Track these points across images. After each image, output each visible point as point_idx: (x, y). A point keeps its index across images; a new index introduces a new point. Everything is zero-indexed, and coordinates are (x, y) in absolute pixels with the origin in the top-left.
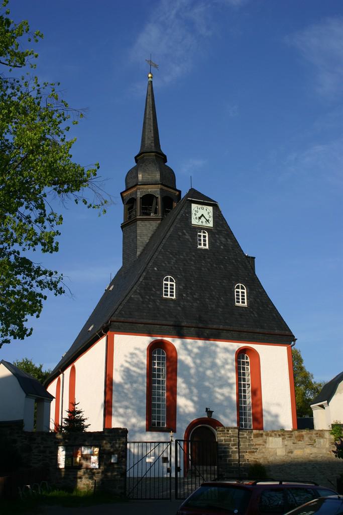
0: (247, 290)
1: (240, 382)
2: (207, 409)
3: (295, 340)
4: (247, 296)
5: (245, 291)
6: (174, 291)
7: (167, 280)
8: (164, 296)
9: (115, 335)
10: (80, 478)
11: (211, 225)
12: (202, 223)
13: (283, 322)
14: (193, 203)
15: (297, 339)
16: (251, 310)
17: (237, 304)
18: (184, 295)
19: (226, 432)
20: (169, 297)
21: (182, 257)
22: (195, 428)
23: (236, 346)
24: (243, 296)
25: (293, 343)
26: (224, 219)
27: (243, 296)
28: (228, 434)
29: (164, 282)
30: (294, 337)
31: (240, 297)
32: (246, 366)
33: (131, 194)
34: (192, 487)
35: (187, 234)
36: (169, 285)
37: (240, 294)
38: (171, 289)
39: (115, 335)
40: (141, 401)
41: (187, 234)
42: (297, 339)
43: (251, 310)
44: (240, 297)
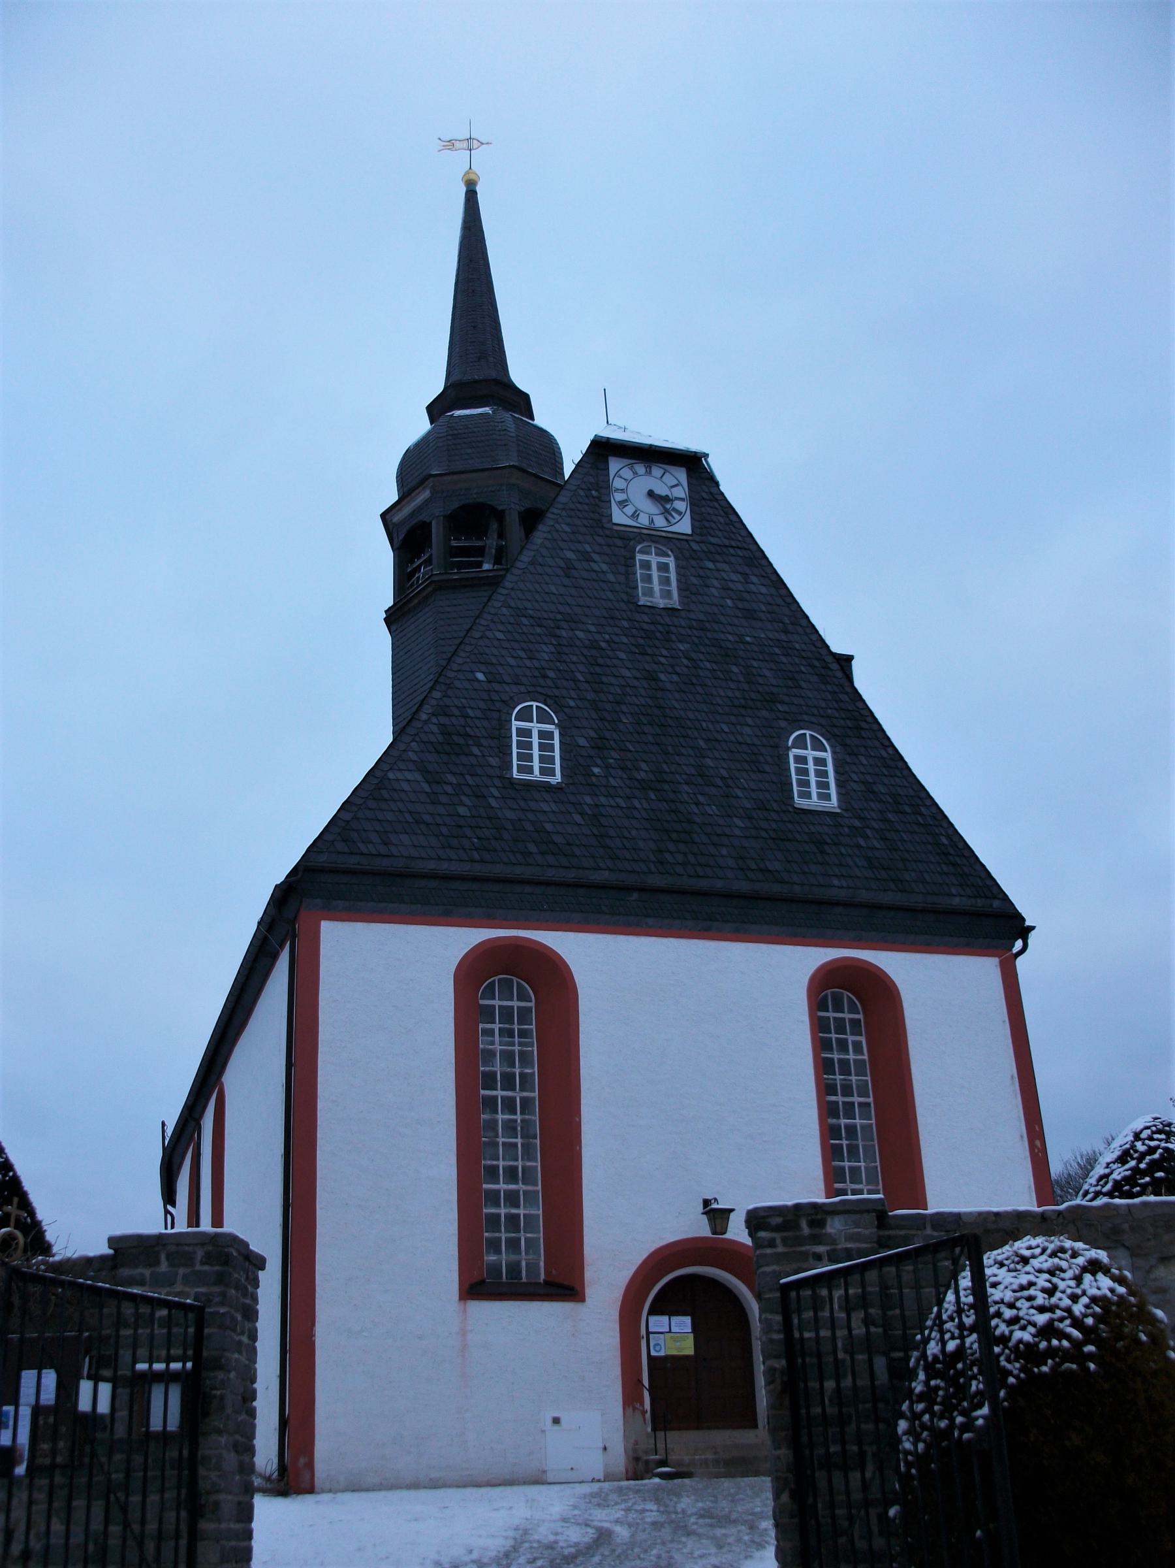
0: (834, 753)
1: (832, 1121)
2: (706, 1203)
3: (1024, 932)
4: (836, 772)
5: (828, 756)
6: (557, 754)
7: (525, 715)
8: (515, 774)
9: (325, 925)
10: (539, 1542)
11: (684, 526)
12: (648, 515)
13: (978, 867)
14: (615, 455)
15: (1033, 928)
16: (857, 823)
17: (799, 802)
18: (596, 770)
19: (806, 1230)
20: (536, 775)
21: (581, 635)
22: (484, 986)
23: (814, 957)
24: (822, 774)
25: (1019, 944)
26: (733, 509)
27: (822, 774)
28: (816, 1239)
29: (515, 724)
30: (1023, 920)
31: (813, 779)
32: (851, 1038)
33: (412, 514)
34: (900, 1447)
35: (596, 557)
36: (535, 734)
37: (811, 767)
38: (542, 747)
39: (325, 925)
40: (765, 1505)
41: (596, 557)
42: (1033, 928)
43: (857, 823)
44: (813, 779)
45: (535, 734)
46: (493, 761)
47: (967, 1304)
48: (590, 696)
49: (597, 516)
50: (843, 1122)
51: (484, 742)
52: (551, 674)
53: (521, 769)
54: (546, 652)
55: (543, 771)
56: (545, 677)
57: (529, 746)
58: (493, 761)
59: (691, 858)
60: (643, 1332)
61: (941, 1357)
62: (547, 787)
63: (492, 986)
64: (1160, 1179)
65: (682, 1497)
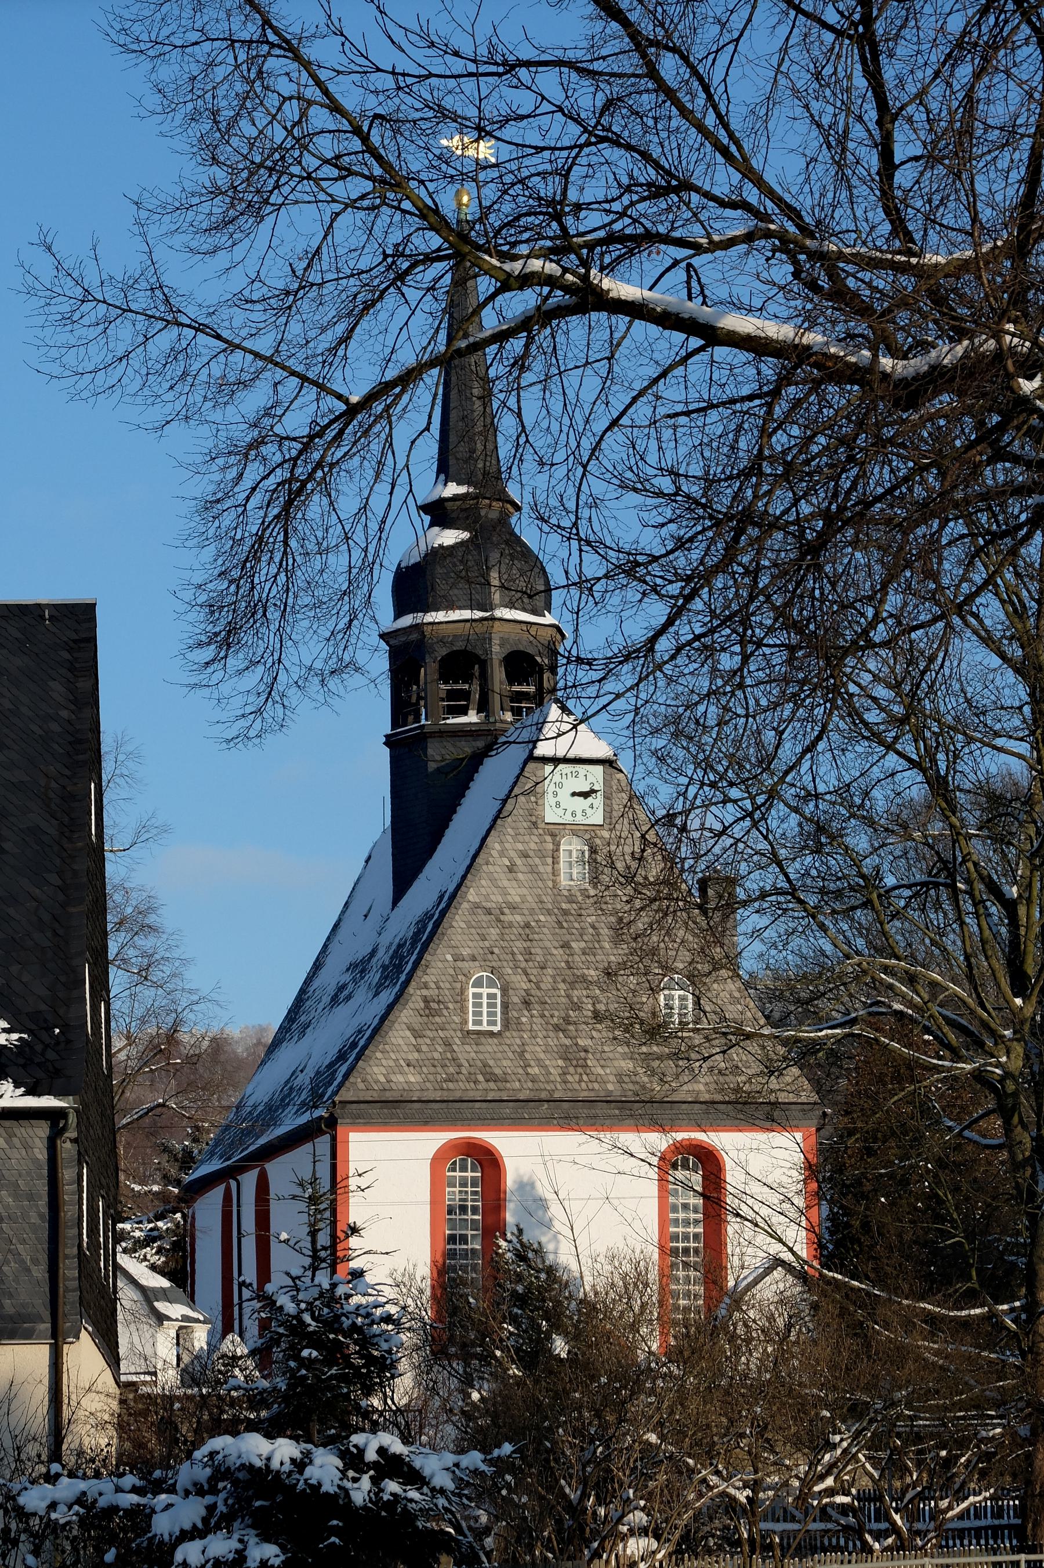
7: (478, 984)
9: (353, 1136)
45: (485, 996)
46: (457, 1019)
47: (916, 1548)
48: (523, 964)
49: (534, 819)
50: (681, 1245)
51: (450, 1006)
52: (496, 950)
53: (475, 1023)
54: (494, 933)
55: (489, 1023)
56: (492, 953)
57: (480, 1005)
58: (457, 1019)
59: (585, 1077)
60: (236, 1300)
61: (25, 1036)
62: (491, 1034)
63: (455, 1163)
64: (928, 1041)
65: (229, 1468)
